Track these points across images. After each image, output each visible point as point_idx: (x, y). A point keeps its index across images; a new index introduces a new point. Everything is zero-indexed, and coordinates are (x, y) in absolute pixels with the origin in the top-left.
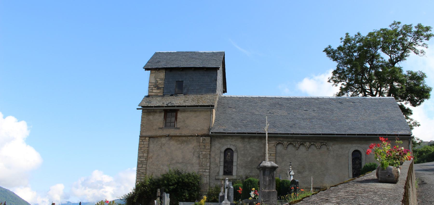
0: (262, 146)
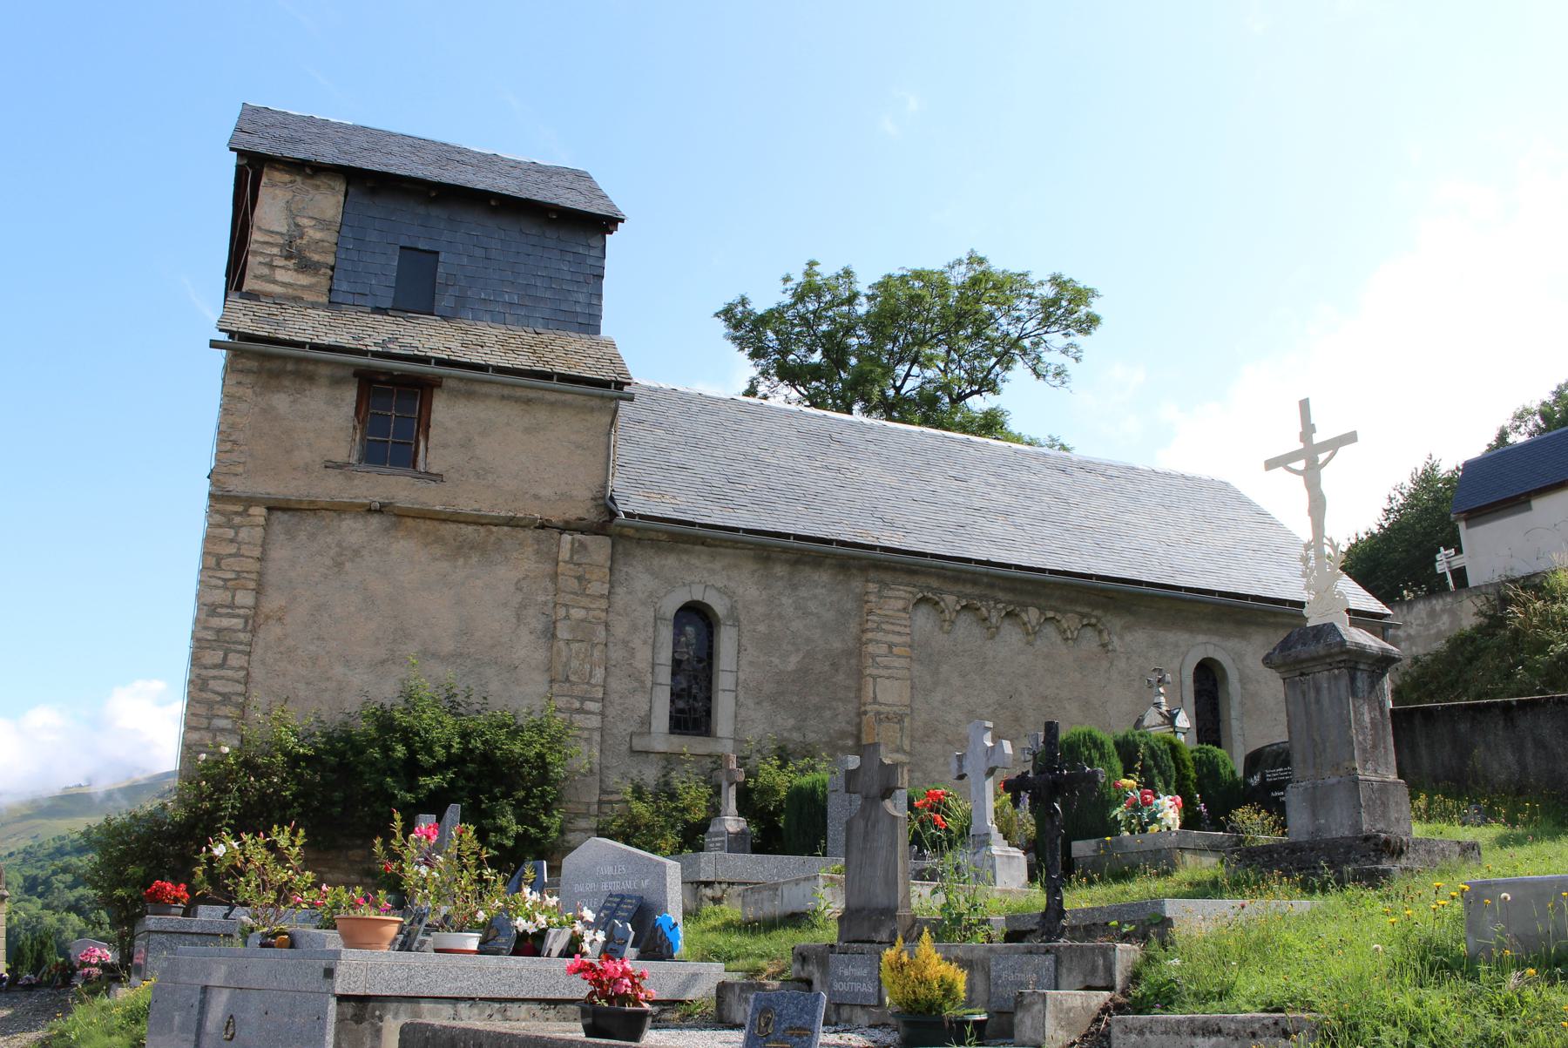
0: (849, 606)
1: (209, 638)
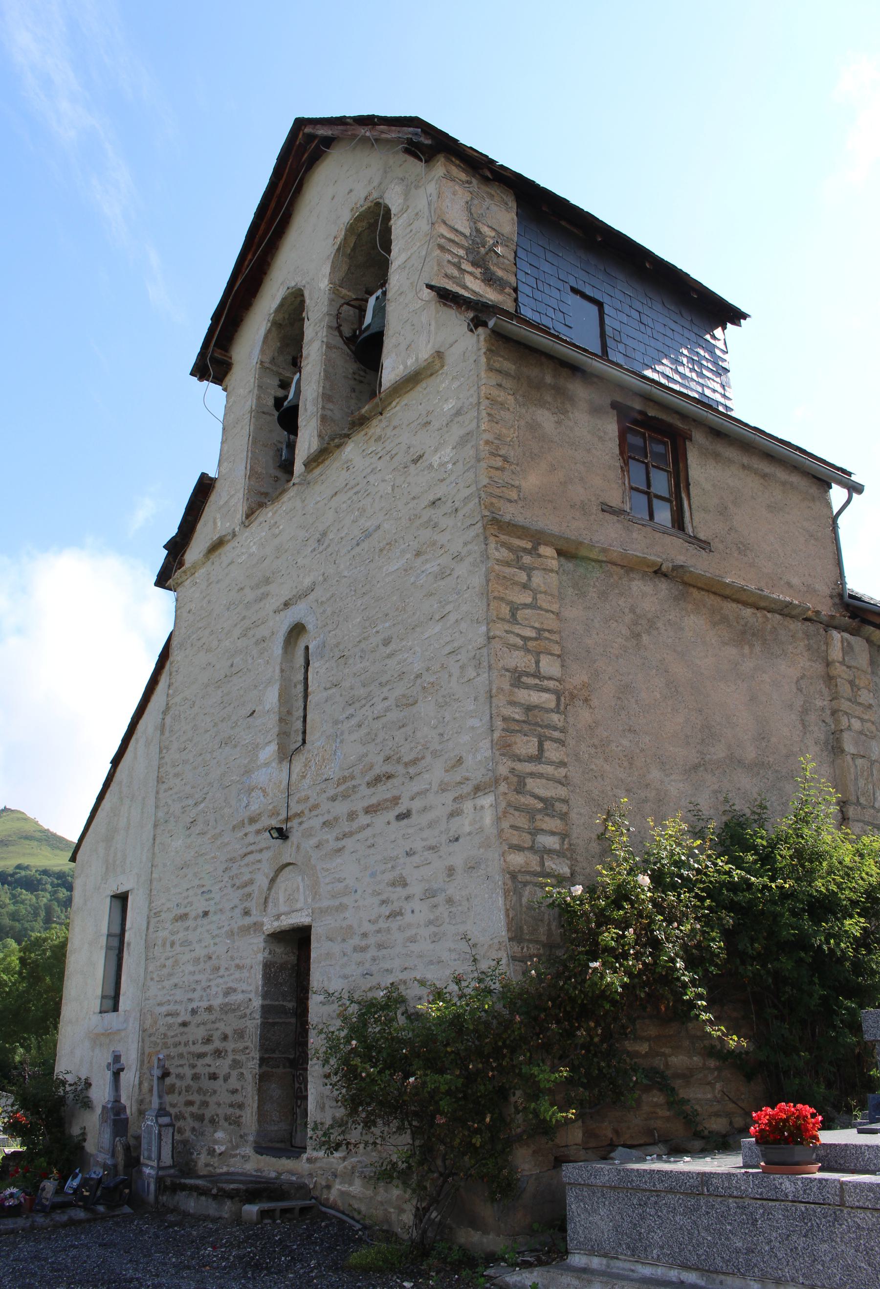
1: (517, 717)
